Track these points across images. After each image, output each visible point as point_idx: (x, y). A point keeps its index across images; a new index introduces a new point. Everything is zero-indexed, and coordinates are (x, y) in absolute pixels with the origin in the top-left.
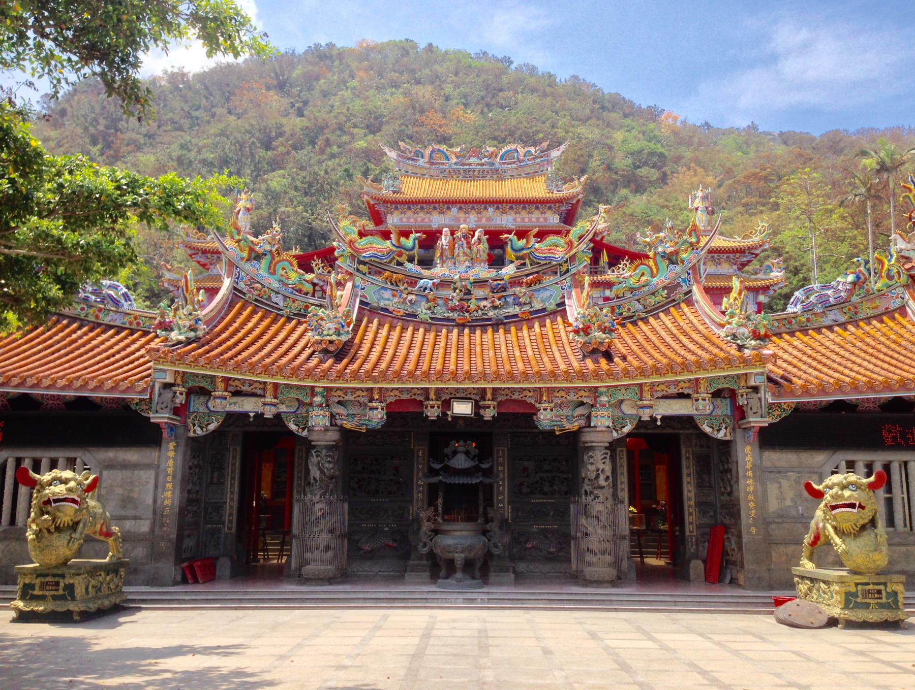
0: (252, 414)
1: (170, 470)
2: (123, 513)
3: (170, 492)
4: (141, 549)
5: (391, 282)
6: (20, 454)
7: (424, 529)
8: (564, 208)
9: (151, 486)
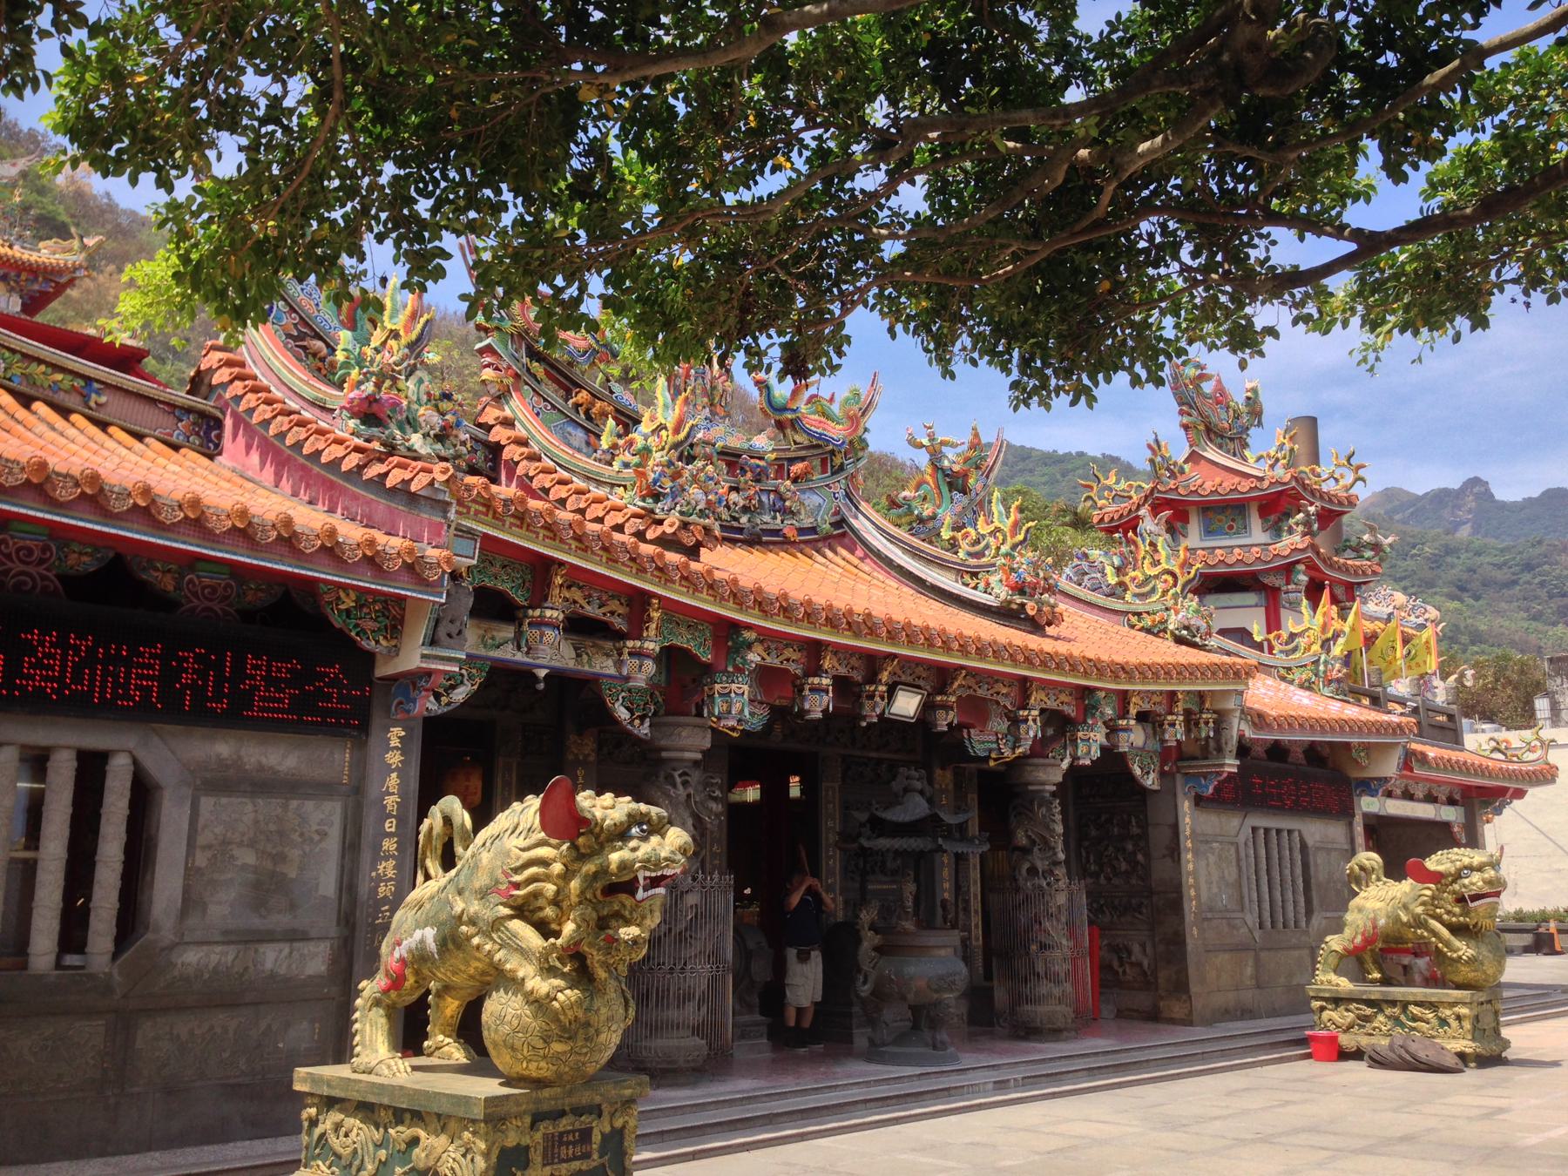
0: (542, 673)
1: (391, 802)
2: (256, 922)
3: (392, 863)
4: (305, 1025)
5: (587, 413)
6: (95, 739)
7: (866, 945)
8: (36, 287)
9: (333, 844)
